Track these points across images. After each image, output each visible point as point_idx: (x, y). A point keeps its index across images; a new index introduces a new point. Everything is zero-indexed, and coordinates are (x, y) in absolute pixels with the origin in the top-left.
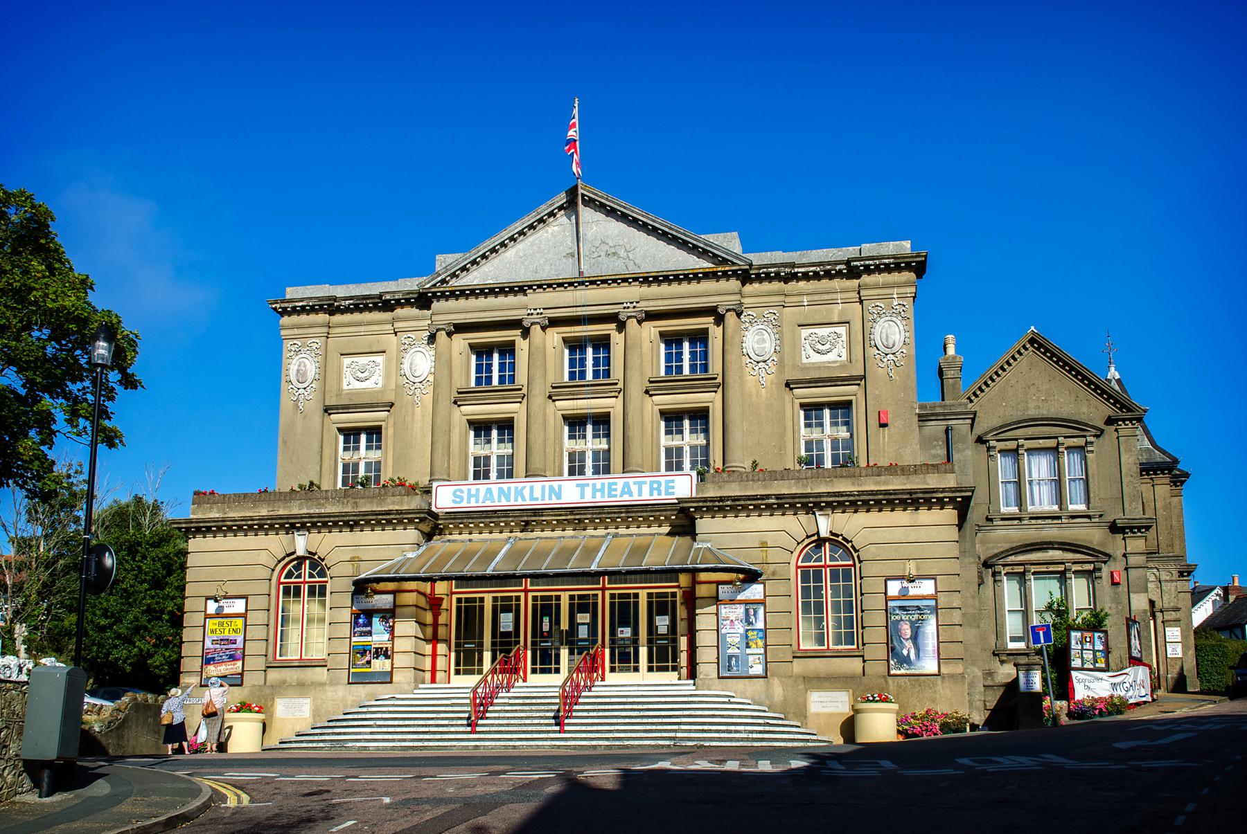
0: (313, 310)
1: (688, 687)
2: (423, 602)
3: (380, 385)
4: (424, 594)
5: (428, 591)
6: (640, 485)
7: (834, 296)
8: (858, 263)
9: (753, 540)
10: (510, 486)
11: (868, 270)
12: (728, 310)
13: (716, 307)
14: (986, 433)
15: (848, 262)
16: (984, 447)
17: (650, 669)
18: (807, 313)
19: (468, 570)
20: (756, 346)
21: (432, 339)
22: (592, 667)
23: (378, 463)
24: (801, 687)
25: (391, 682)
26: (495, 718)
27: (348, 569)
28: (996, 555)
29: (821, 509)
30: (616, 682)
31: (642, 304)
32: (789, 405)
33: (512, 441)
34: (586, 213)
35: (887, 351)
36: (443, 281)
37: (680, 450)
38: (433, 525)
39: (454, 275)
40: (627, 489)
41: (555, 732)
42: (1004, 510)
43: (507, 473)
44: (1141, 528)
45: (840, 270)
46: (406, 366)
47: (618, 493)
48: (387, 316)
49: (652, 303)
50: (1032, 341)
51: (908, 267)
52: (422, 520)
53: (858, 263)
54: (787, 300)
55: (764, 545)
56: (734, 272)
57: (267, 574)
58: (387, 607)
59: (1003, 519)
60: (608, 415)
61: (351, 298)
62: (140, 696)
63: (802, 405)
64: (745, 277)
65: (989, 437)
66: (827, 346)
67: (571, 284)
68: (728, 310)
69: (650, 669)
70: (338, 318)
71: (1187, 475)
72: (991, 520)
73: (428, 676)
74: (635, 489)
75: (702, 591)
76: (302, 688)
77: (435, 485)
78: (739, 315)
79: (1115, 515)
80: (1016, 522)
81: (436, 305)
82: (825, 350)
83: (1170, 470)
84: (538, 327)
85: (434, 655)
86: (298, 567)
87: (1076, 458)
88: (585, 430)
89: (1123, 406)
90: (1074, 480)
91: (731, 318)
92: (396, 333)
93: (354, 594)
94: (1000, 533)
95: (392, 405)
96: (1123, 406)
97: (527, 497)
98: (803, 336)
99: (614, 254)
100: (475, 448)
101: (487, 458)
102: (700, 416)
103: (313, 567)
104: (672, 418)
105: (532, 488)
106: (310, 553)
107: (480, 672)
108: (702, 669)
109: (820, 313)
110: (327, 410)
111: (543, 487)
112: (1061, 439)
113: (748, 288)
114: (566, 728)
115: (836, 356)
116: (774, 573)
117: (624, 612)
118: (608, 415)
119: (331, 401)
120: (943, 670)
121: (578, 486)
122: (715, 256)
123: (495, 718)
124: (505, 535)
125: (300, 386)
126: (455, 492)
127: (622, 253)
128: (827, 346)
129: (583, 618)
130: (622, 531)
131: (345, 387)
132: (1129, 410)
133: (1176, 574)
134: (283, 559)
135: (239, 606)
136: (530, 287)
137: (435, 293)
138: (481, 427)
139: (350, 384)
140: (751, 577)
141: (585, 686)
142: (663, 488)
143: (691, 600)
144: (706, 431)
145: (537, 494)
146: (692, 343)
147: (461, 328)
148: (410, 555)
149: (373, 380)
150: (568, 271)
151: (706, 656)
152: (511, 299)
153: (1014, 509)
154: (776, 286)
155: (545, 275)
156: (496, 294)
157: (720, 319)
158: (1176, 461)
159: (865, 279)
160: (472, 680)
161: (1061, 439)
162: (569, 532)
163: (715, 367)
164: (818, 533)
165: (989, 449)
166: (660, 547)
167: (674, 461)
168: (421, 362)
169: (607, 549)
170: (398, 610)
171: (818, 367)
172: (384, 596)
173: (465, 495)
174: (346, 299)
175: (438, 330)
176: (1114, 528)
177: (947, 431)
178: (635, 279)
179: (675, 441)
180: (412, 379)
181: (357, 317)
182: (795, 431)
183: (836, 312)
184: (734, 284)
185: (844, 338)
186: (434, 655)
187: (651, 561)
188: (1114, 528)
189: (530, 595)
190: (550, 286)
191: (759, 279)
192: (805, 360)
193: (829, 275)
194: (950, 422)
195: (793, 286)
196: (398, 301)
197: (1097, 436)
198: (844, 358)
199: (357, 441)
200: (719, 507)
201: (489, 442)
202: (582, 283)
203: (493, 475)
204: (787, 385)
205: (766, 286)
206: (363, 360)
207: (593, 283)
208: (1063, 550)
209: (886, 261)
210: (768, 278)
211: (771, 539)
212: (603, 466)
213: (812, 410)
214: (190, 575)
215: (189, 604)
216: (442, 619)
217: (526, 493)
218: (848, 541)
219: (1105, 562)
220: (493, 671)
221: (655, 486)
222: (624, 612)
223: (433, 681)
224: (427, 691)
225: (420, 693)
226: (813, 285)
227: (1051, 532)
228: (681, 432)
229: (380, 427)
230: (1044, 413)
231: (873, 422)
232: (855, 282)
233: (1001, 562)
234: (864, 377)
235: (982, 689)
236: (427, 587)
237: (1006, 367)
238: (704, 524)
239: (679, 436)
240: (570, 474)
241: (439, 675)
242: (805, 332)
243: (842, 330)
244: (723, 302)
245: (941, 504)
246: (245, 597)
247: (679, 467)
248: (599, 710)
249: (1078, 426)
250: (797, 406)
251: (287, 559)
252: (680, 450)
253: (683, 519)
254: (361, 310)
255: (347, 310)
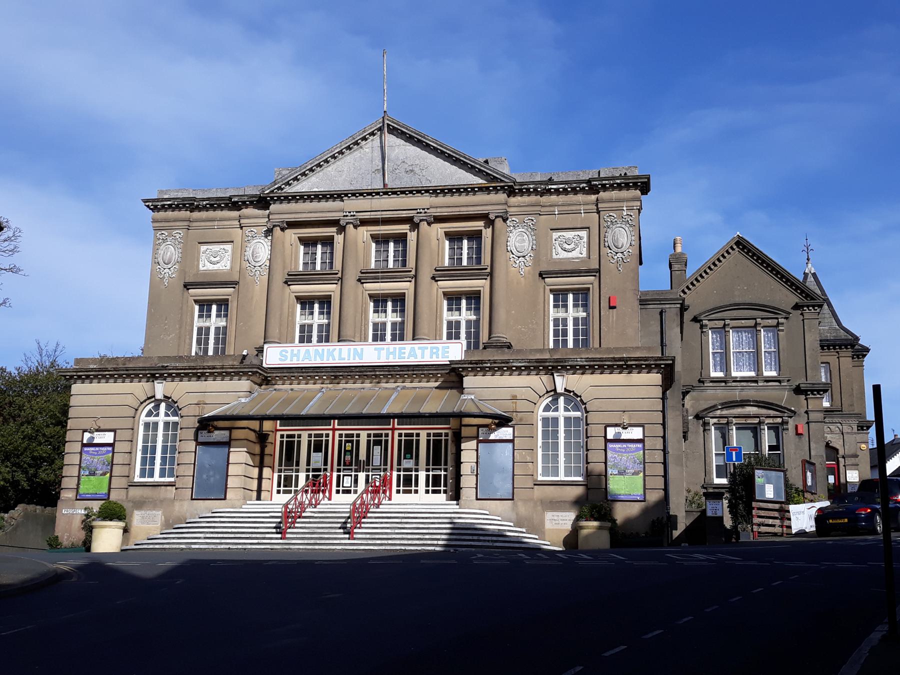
0: (178, 207)
1: (453, 506)
2: (252, 436)
3: (228, 267)
4: (254, 431)
5: (258, 429)
6: (423, 349)
7: (578, 207)
8: (597, 183)
9: (506, 394)
10: (325, 348)
11: (604, 188)
12: (496, 217)
13: (488, 214)
14: (701, 314)
15: (589, 182)
16: (698, 325)
17: (427, 492)
18: (558, 221)
19: (288, 411)
20: (517, 244)
21: (269, 232)
22: (378, 489)
23: (225, 328)
24: (540, 508)
25: (225, 499)
26: (301, 528)
27: (195, 411)
28: (706, 409)
29: (558, 371)
30: (400, 501)
31: (431, 210)
32: (542, 290)
33: (226, 316)
34: (391, 140)
35: (520, 254)
36: (280, 188)
37: (458, 323)
38: (266, 378)
39: (288, 184)
40: (413, 353)
41: (277, 539)
42: (713, 374)
43: (325, 338)
44: (821, 390)
45: (584, 188)
46: (249, 253)
47: (406, 355)
48: (235, 214)
49: (439, 210)
50: (738, 243)
51: (635, 186)
52: (254, 373)
53: (597, 183)
54: (191, 224)
55: (514, 398)
56: (502, 187)
57: (131, 412)
58: (224, 440)
59: (711, 382)
60: (404, 295)
61: (208, 199)
62: (31, 507)
63: (551, 291)
64: (511, 191)
65: (702, 317)
66: (572, 246)
67: (378, 194)
68: (496, 217)
69: (427, 492)
70: (196, 215)
71: (868, 350)
72: (703, 382)
73: (255, 494)
74: (419, 352)
75: (465, 432)
76: (154, 504)
77: (266, 346)
78: (505, 220)
79: (800, 381)
80: (723, 384)
81: (273, 207)
82: (571, 247)
83: (853, 346)
84: (351, 226)
85: (260, 478)
86: (157, 407)
87: (745, 336)
88: (386, 307)
89: (807, 296)
90: (769, 353)
91: (499, 222)
92: (241, 228)
93: (198, 430)
94: (710, 392)
95: (237, 283)
96: (807, 296)
97: (337, 358)
98: (554, 237)
99: (412, 171)
100: (300, 318)
101: (311, 326)
102: (474, 297)
103: (169, 407)
104: (453, 299)
105: (341, 349)
106: (165, 397)
107: (356, 492)
108: (464, 493)
109: (569, 220)
110: (187, 286)
111: (349, 350)
112: (759, 320)
113: (514, 200)
114: (288, 536)
115: (579, 253)
116: (521, 420)
117: (409, 448)
118: (404, 295)
119: (544, 268)
120: (648, 497)
121: (375, 349)
122: (488, 174)
123: (301, 528)
124: (318, 386)
125: (166, 266)
126: (282, 351)
127: (417, 170)
128: (572, 246)
129: (377, 450)
130: (408, 385)
131: (201, 268)
132: (812, 299)
133: (855, 428)
134: (145, 401)
135: (108, 438)
136: (346, 195)
137: (272, 198)
138: (306, 302)
139: (205, 266)
140: (503, 421)
141: (310, 504)
142: (440, 353)
143: (458, 439)
144: (403, 311)
145: (345, 354)
146: (396, 242)
147: (292, 225)
148: (243, 400)
149: (222, 263)
150: (378, 185)
151: (468, 481)
152: (330, 204)
153: (720, 374)
154: (533, 198)
155: (365, 186)
156: (320, 200)
157: (490, 223)
158: (857, 339)
159: (602, 194)
160: (285, 498)
161: (759, 320)
162: (367, 385)
163: (486, 260)
164: (555, 390)
165: (702, 327)
166: (436, 400)
167: (453, 333)
168: (261, 249)
169: (394, 398)
170: (233, 443)
171: (561, 261)
172: (222, 432)
173: (289, 355)
174: (204, 200)
175: (274, 226)
176: (798, 391)
177: (661, 313)
178: (427, 191)
179: (455, 317)
180: (253, 263)
181: (211, 214)
182: (438, 316)
183: (578, 220)
184: (502, 196)
185: (585, 240)
186: (260, 478)
187: (428, 408)
188: (798, 391)
189: (396, 433)
190: (361, 194)
191: (521, 193)
192: (554, 256)
193: (575, 191)
194: (664, 306)
195: (545, 199)
196: (244, 203)
197: (787, 318)
198: (585, 255)
199: (209, 310)
200: (478, 367)
201: (312, 313)
202: (386, 193)
203: (315, 338)
204: (541, 275)
205: (526, 199)
206: (216, 248)
207: (394, 193)
208: (759, 407)
209: (618, 181)
210: (528, 192)
211: (520, 393)
212: (399, 335)
213: (560, 295)
214: (72, 413)
215: (69, 436)
216: (268, 450)
217: (336, 354)
218: (578, 396)
219: (791, 417)
220: (366, 491)
221: (435, 350)
222: (409, 448)
223: (259, 498)
224: (253, 506)
225: (246, 508)
226: (562, 199)
227: (751, 393)
228: (459, 310)
229: (228, 300)
230: (748, 299)
231: (605, 304)
232: (593, 197)
233: (711, 415)
234: (599, 271)
235: (684, 514)
236: (255, 425)
237: (717, 263)
238: (469, 381)
239: (457, 313)
240: (448, 339)
241: (263, 494)
242: (555, 235)
243: (584, 234)
244: (493, 211)
245: (649, 369)
246: (114, 431)
247: (458, 337)
248: (382, 523)
249: (773, 311)
250: (547, 291)
251: (148, 402)
252: (458, 323)
253: (452, 376)
254: (215, 209)
255: (205, 208)
